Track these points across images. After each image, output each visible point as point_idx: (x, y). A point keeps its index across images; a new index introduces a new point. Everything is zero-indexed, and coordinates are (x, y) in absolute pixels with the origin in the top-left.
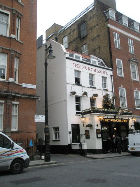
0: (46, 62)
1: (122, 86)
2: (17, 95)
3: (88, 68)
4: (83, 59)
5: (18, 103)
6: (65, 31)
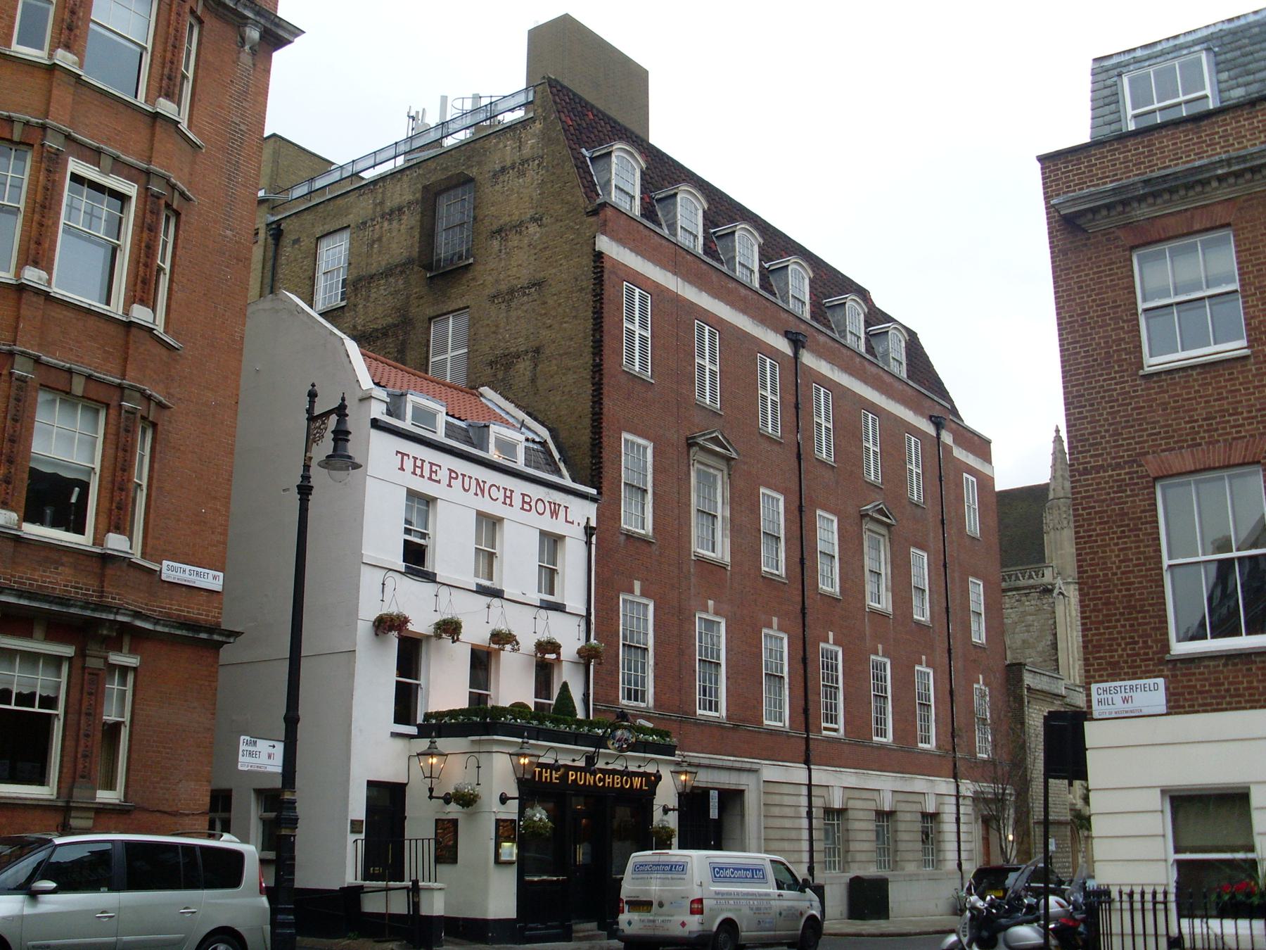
0: (306, 477)
1: (637, 586)
2: (138, 623)
3: (474, 482)
4: (451, 420)
5: (132, 661)
6: (340, 202)
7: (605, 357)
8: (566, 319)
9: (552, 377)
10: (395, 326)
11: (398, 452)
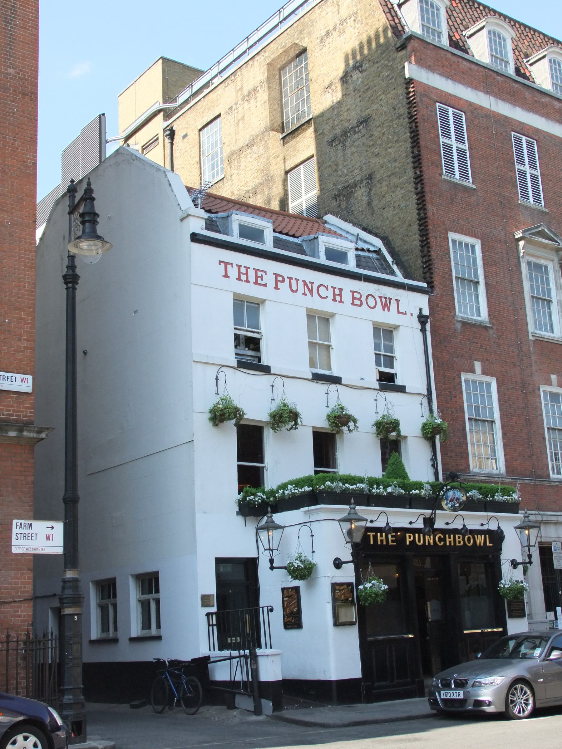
1: (478, 366)
3: (301, 284)
4: (277, 235)
7: (424, 168)
8: (390, 145)
9: (384, 196)
10: (261, 184)
11: (220, 262)
